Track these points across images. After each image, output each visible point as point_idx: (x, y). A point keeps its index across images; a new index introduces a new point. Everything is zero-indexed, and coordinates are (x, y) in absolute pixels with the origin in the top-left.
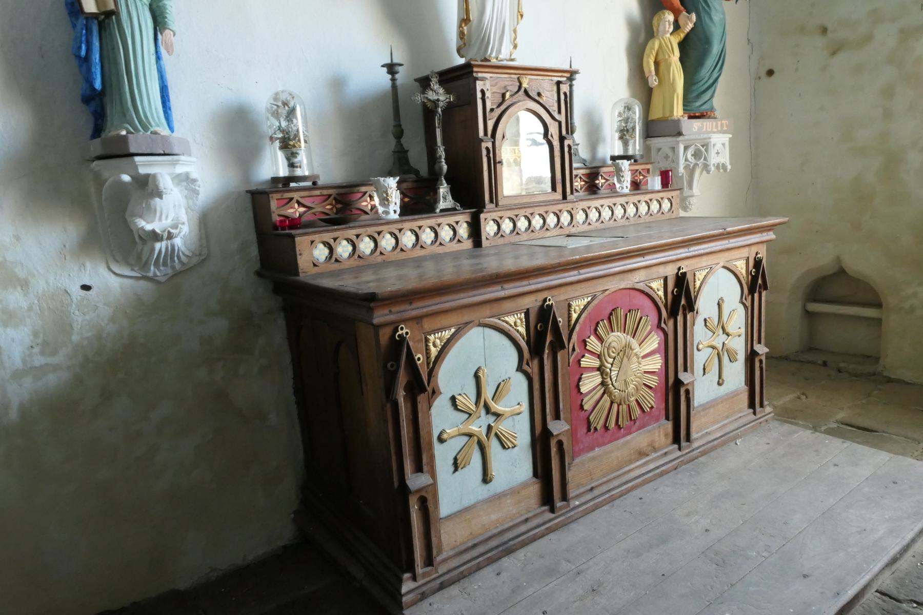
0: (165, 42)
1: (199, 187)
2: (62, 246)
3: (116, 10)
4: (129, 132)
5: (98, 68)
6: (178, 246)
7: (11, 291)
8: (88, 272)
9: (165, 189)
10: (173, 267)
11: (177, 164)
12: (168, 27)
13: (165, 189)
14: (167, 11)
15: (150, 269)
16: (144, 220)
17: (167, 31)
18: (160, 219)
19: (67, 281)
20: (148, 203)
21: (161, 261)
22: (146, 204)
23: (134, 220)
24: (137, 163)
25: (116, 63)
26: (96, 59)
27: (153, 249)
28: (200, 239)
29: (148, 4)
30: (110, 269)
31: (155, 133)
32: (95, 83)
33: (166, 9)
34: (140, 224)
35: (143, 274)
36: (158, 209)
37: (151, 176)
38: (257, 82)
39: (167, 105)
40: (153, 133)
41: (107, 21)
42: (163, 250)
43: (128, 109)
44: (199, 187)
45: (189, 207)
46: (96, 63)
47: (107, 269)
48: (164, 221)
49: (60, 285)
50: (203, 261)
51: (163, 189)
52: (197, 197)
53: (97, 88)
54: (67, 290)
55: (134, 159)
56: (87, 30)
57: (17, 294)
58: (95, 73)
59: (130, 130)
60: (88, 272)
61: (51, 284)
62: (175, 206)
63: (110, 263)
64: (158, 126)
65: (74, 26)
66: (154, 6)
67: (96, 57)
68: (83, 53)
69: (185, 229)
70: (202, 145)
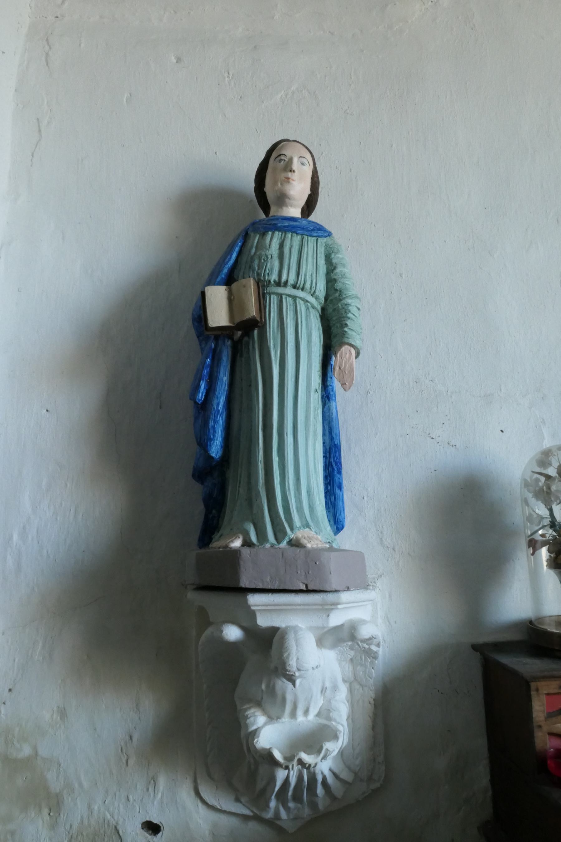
0: (340, 368)
1: (378, 645)
2: (128, 737)
3: (258, 319)
4: (247, 543)
5: (221, 421)
6: (322, 773)
7: (33, 815)
8: (160, 795)
9: (299, 670)
10: (313, 805)
11: (332, 609)
12: (346, 340)
13: (299, 670)
14: (350, 315)
15: (268, 806)
16: (265, 712)
17: (345, 348)
18: (293, 715)
19: (122, 809)
20: (272, 683)
21: (290, 793)
22: (268, 686)
23: (246, 710)
24: (253, 608)
25: (251, 409)
26: (218, 405)
27: (273, 779)
28: (374, 744)
29: (319, 308)
30: (197, 793)
31: (295, 544)
32: (210, 446)
33: (347, 311)
34: (253, 724)
35: (255, 811)
36: (289, 698)
37: (280, 631)
38: (502, 431)
39: (336, 479)
40: (293, 542)
41: (246, 339)
42: (293, 781)
43: (258, 494)
44: (378, 645)
45: (355, 679)
46: (218, 411)
47: (193, 793)
48: (300, 718)
49: (108, 816)
50: (376, 791)
51: (294, 669)
52: (372, 663)
53: (213, 455)
54: (118, 827)
55: (246, 601)
56: (213, 359)
57: (41, 822)
58: (214, 428)
59: (250, 539)
60: (160, 795)
61: (95, 812)
62: (323, 690)
63: (199, 781)
64: (307, 526)
65: (202, 350)
66: (330, 310)
67: (220, 401)
68: (201, 396)
69: (343, 740)
70: (394, 550)
